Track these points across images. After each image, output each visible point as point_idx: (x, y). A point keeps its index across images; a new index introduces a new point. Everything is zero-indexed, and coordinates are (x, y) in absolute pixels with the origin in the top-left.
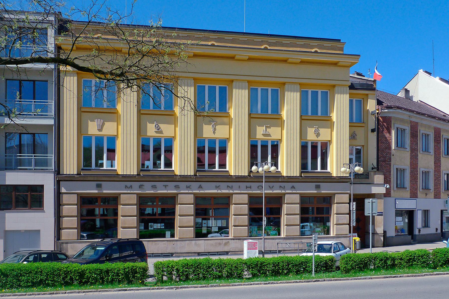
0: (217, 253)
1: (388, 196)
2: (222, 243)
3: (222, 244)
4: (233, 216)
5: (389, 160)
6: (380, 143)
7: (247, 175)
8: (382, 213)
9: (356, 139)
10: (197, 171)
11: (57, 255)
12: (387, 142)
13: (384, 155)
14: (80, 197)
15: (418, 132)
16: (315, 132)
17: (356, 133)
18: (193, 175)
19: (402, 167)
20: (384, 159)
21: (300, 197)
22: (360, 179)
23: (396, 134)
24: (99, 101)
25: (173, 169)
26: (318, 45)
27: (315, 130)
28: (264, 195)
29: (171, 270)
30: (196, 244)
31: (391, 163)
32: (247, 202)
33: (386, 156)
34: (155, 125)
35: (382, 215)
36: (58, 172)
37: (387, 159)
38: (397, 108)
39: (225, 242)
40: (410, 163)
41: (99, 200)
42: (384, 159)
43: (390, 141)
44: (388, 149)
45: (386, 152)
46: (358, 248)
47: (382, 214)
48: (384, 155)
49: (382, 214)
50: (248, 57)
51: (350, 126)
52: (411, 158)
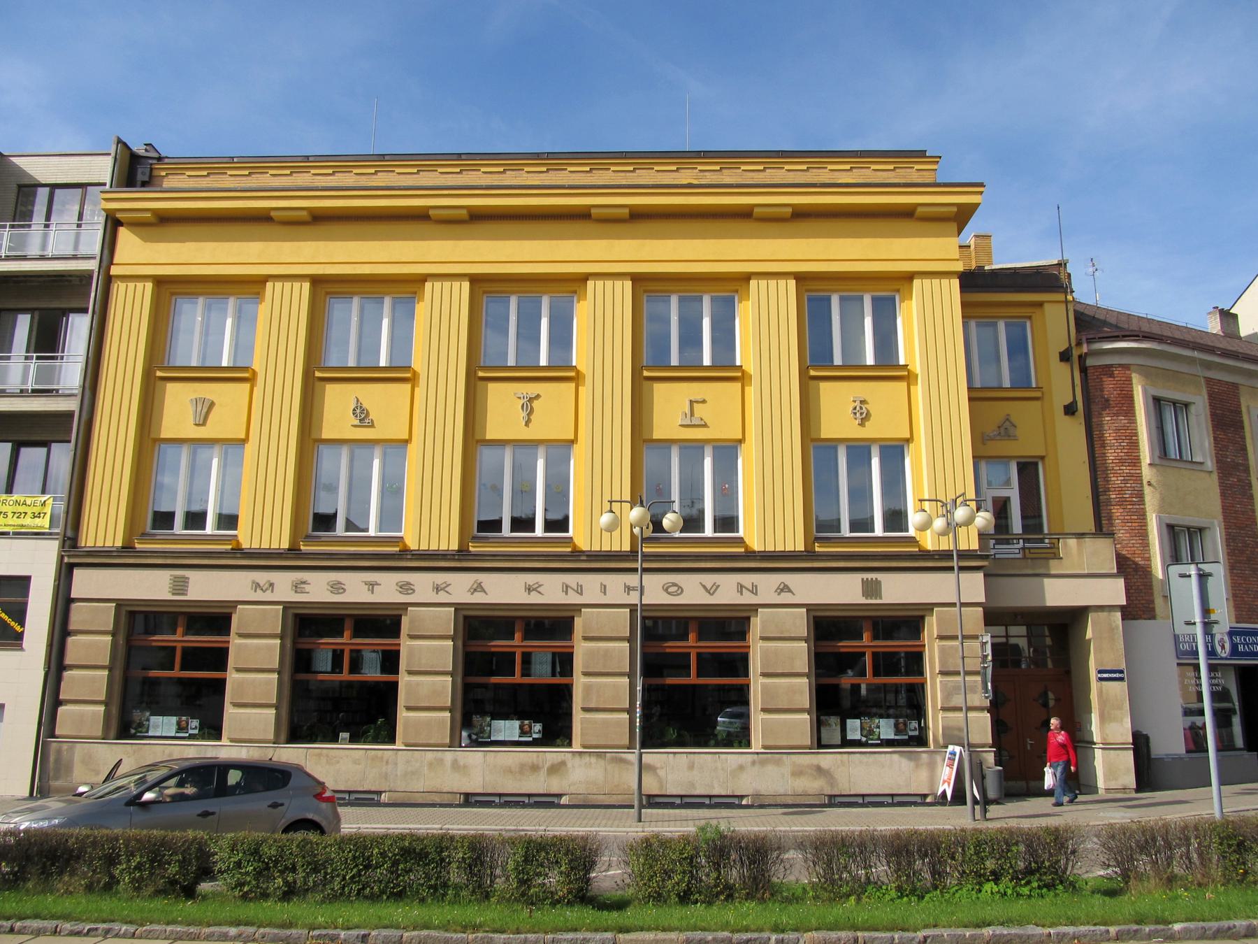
0: (678, 801)
1: (1145, 616)
2: (541, 764)
3: (543, 767)
4: (939, 679)
5: (1134, 499)
6: (1099, 445)
7: (803, 550)
8: (1121, 672)
9: (1015, 438)
10: (817, 539)
11: (324, 796)
12: (1122, 444)
13: (1116, 482)
14: (296, 615)
15: (1240, 412)
16: (855, 414)
17: (1013, 419)
18: (803, 551)
19: (1194, 520)
20: (1118, 496)
21: (123, 619)
22: (1029, 560)
23: (1158, 416)
24: (691, 339)
25: (570, 534)
26: (851, 167)
27: (855, 408)
28: (642, 610)
29: (396, 852)
30: (455, 765)
31: (1144, 509)
32: (628, 635)
33: (1123, 485)
34: (354, 410)
35: (1121, 679)
36: (70, 542)
37: (1128, 496)
38: (1143, 337)
39: (550, 763)
40: (1223, 509)
41: (348, 625)
42: (1118, 496)
43: (1134, 438)
44: (1127, 464)
45: (1123, 473)
46: (992, 794)
47: (1121, 675)
48: (1116, 482)
49: (1121, 675)
50: (790, 210)
51: (970, 399)
52: (1223, 495)
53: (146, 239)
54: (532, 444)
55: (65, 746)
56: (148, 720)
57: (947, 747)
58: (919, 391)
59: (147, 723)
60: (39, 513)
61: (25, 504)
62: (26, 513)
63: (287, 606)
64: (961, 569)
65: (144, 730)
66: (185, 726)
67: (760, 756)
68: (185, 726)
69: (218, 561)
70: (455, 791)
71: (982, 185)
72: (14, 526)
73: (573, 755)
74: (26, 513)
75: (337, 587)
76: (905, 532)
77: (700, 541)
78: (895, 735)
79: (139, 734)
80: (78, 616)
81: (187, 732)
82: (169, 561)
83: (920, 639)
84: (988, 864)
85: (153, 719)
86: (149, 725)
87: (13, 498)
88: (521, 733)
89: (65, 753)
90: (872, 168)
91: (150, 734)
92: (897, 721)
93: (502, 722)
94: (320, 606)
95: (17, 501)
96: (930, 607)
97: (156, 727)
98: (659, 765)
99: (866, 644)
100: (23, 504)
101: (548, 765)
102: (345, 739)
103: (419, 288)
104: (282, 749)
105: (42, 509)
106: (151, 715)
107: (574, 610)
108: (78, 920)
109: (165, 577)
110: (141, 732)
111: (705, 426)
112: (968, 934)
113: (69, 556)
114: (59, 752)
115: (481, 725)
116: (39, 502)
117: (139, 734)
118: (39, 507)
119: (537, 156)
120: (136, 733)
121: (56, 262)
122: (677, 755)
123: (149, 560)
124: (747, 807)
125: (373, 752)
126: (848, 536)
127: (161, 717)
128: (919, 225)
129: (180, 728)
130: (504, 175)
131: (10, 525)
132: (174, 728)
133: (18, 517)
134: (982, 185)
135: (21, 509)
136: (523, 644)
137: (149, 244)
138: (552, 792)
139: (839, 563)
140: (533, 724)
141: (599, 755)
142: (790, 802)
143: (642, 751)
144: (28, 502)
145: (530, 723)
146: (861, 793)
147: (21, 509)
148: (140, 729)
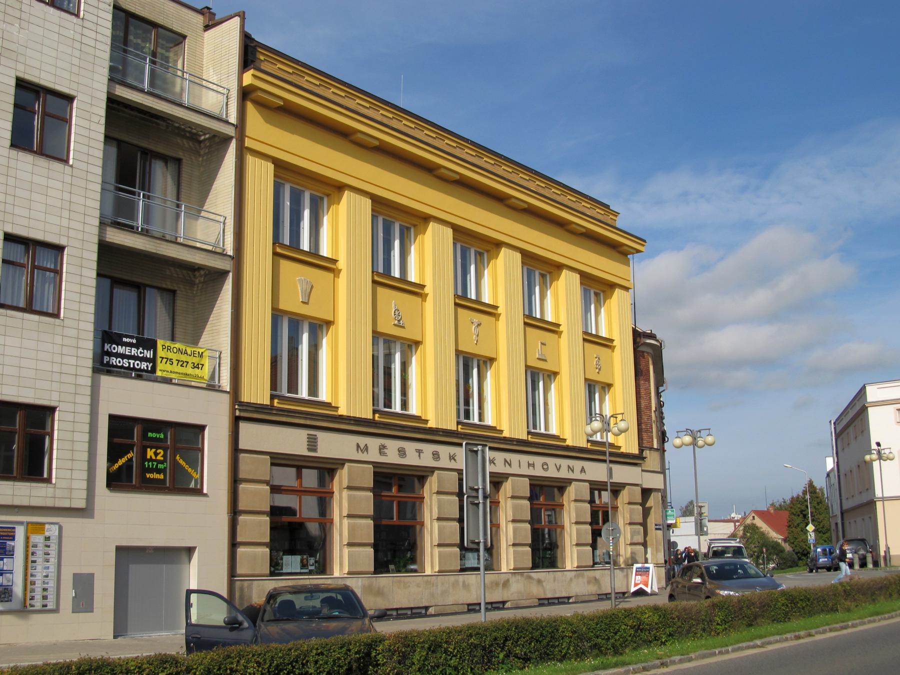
53: (267, 121)
54: (396, 338)
55: (246, 584)
56: (282, 559)
57: (633, 565)
58: (342, 281)
59: (281, 562)
60: (198, 364)
61: (187, 353)
62: (188, 362)
63: (375, 464)
64: (611, 462)
65: (280, 568)
66: (306, 563)
67: (578, 572)
68: (306, 563)
69: (447, 440)
70: (461, 602)
71: (645, 241)
72: (179, 373)
73: (512, 575)
74: (188, 362)
75: (545, 467)
76: (296, 394)
77: (291, 400)
78: (301, 569)
79: (276, 572)
80: (246, 465)
81: (308, 569)
82: (308, 422)
83: (41, 473)
84: (335, 669)
85: (285, 557)
86: (282, 563)
87: (176, 346)
88: (302, 566)
89: (246, 589)
90: (582, 204)
91: (284, 571)
92: (302, 557)
93: (290, 557)
94: (283, 457)
95: (179, 349)
96: (341, 463)
97: (287, 565)
98: (543, 580)
99: (395, 494)
100: (185, 353)
101: (502, 582)
102: (393, 570)
103: (493, 248)
104: (380, 578)
105: (200, 361)
106: (283, 555)
107: (502, 477)
108: (883, 614)
109: (302, 435)
110: (278, 570)
111: (545, 360)
112: (821, 630)
113: (240, 410)
114: (242, 589)
115: (277, 559)
116: (197, 353)
117: (276, 572)
118: (197, 358)
119: (473, 143)
120: (274, 570)
121: (202, 117)
122: (550, 573)
123: (316, 422)
124: (508, 609)
125: (398, 578)
126: (307, 398)
127: (290, 556)
128: (352, 146)
129: (304, 565)
130: (434, 140)
131: (177, 373)
132: (299, 565)
133: (181, 366)
134: (645, 241)
135: (183, 358)
136: (399, 495)
137: (268, 126)
138: (403, 607)
139: (528, 448)
140: (309, 558)
141: (522, 574)
142: (587, 599)
143: (486, 572)
144: (189, 352)
145: (307, 557)
146: (395, 607)
147: (183, 358)
148: (277, 567)
